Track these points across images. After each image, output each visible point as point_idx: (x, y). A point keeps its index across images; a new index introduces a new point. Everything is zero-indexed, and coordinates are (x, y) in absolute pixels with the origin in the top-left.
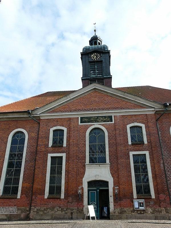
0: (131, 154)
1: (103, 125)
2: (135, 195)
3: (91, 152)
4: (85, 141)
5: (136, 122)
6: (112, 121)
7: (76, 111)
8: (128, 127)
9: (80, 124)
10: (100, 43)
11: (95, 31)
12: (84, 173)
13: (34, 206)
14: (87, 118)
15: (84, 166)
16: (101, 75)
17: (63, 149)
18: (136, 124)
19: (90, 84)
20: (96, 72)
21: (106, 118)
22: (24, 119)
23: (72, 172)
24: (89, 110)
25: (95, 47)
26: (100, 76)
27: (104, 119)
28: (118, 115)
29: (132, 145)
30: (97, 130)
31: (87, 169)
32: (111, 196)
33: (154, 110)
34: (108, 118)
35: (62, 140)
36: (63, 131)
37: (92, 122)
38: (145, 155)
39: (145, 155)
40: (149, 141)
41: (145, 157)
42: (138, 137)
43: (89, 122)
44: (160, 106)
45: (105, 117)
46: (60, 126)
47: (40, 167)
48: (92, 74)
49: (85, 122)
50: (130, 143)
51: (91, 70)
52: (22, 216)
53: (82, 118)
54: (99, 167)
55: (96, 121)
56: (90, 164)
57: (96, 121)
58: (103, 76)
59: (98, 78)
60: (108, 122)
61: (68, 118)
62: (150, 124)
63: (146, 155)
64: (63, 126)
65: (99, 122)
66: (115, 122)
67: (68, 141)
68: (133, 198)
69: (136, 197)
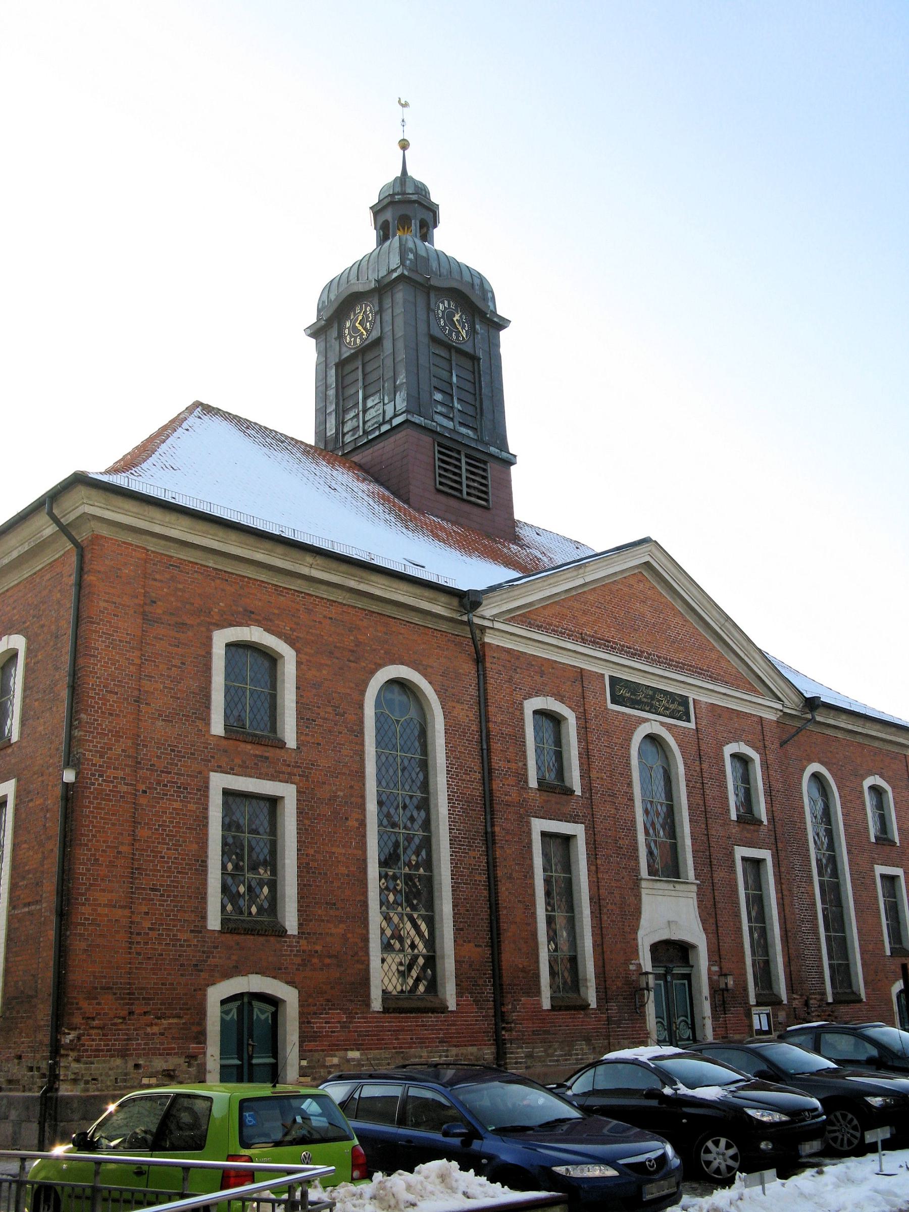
1: (669, 727)
11: (404, 145)
12: (637, 912)
16: (470, 433)
17: (573, 804)
22: (416, 620)
24: (633, 655)
28: (705, 698)
31: (645, 899)
33: (781, 711)
40: (772, 819)
42: (243, 699)
44: (796, 700)
47: (515, 875)
52: (182, 1115)
54: (673, 893)
55: (652, 706)
61: (574, 667)
62: (771, 757)
63: (287, 801)
66: (696, 723)
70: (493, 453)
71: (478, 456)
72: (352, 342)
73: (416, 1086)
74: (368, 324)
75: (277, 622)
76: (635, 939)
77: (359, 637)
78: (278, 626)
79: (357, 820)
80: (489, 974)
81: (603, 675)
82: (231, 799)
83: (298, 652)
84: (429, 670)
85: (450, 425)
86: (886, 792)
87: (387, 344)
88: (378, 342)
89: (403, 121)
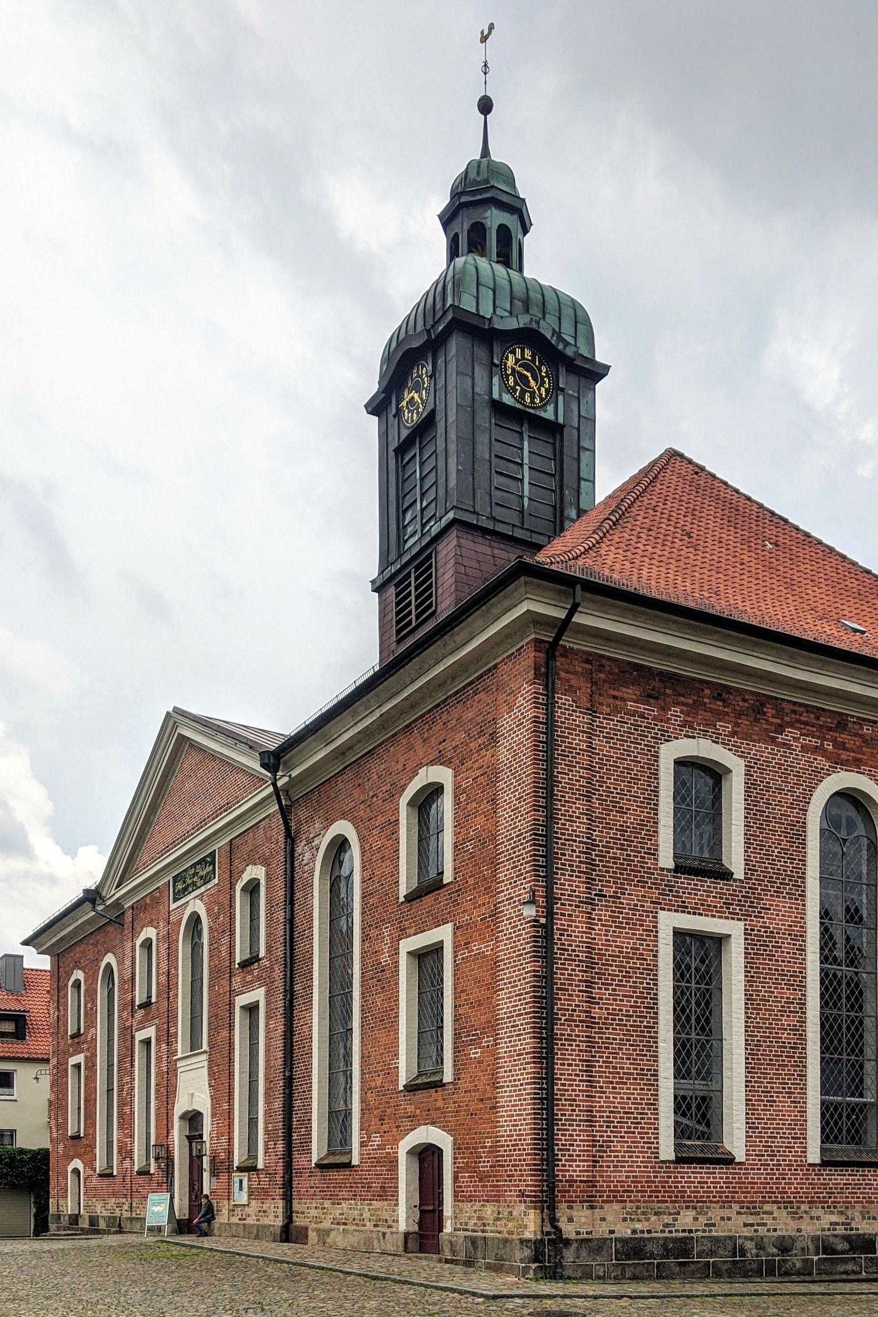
11: (485, 106)
72: (411, 418)
73: (89, 922)
74: (424, 392)
81: (840, 817)
83: (420, 765)
86: (410, 804)
87: (440, 416)
88: (432, 414)
89: (485, 65)
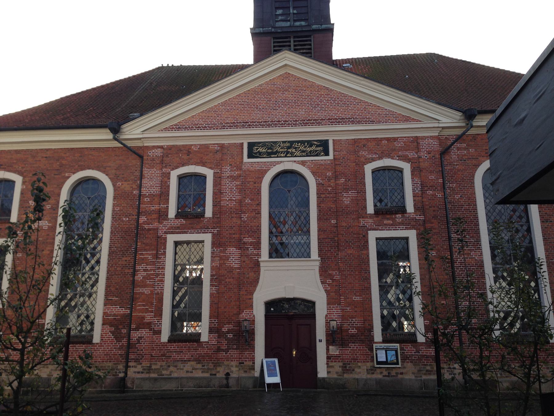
0: (373, 236)
1: (303, 163)
2: (378, 335)
3: (274, 230)
4: (259, 204)
5: (389, 156)
6: (327, 154)
7: (237, 127)
8: (368, 168)
9: (246, 159)
10: (32, 287)
12: (256, 281)
13: (137, 360)
14: (264, 144)
15: (257, 264)
16: (303, 23)
18: (387, 162)
19: (275, 51)
20: (291, 11)
21: (313, 148)
23: (227, 280)
25: (9, 274)
26: (301, 26)
27: (309, 149)
29: (375, 214)
30: (289, 176)
32: (320, 341)
34: (317, 146)
35: (201, 201)
36: (202, 178)
37: (275, 154)
38: (407, 239)
39: (407, 239)
41: (406, 246)
43: (269, 155)
45: (310, 143)
46: (197, 164)
48: (280, 18)
49: (260, 155)
50: (370, 209)
51: (277, 5)
53: (251, 145)
55: (288, 152)
56: (271, 259)
57: (288, 152)
58: (309, 25)
59: (294, 29)
60: (317, 155)
64: (204, 164)
65: (296, 156)
66: (334, 155)
67: (216, 204)
68: (371, 340)
69: (381, 339)
70: (315, 28)
71: (299, 34)
75: (14, 166)
76: (251, 299)
77: (63, 162)
78: (15, 168)
79: (49, 250)
80: (127, 322)
82: (378, 241)
83: (24, 177)
84: (107, 168)
85: (288, 24)
